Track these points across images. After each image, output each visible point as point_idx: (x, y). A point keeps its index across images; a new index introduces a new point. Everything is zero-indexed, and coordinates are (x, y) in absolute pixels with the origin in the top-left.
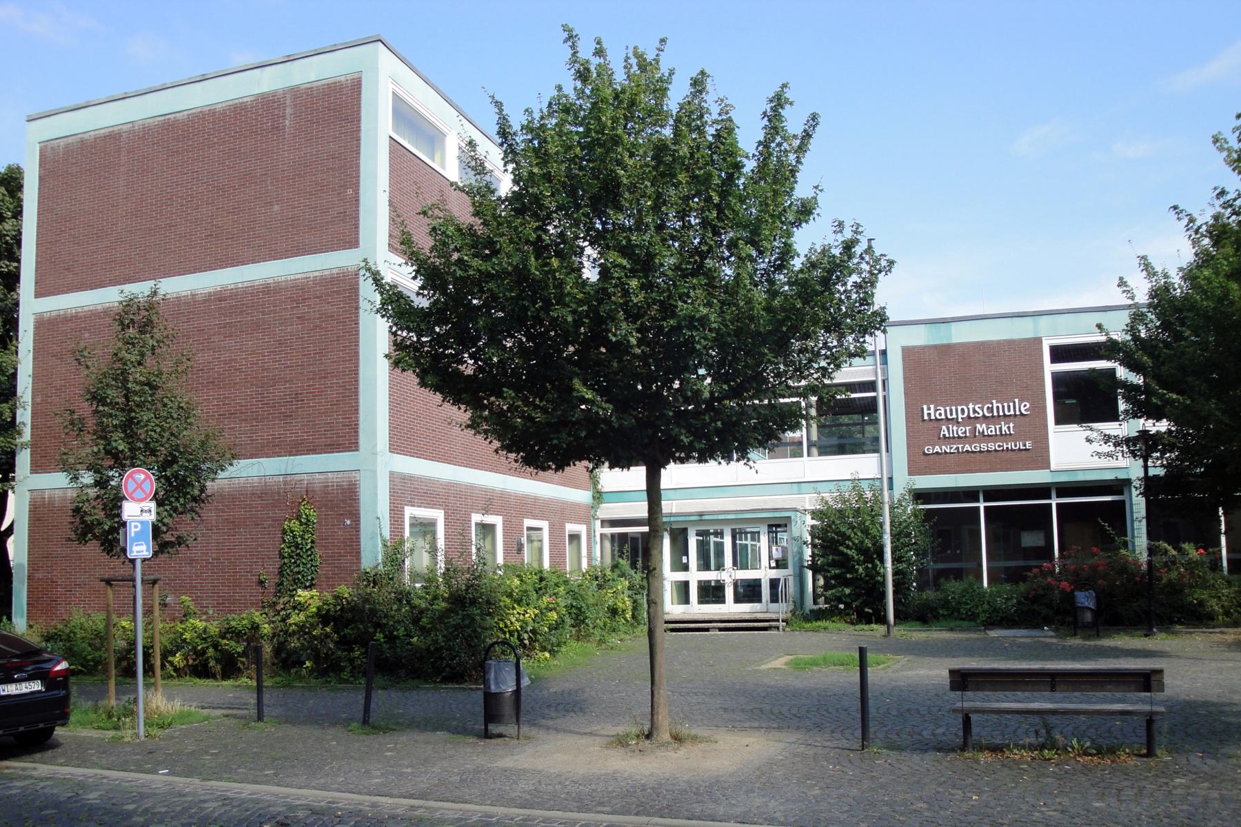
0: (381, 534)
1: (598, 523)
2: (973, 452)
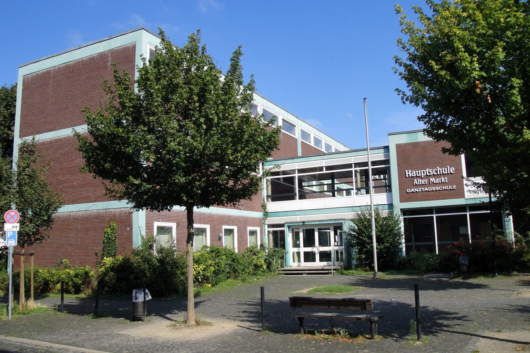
0: (141, 234)
1: (266, 226)
2: (429, 191)
